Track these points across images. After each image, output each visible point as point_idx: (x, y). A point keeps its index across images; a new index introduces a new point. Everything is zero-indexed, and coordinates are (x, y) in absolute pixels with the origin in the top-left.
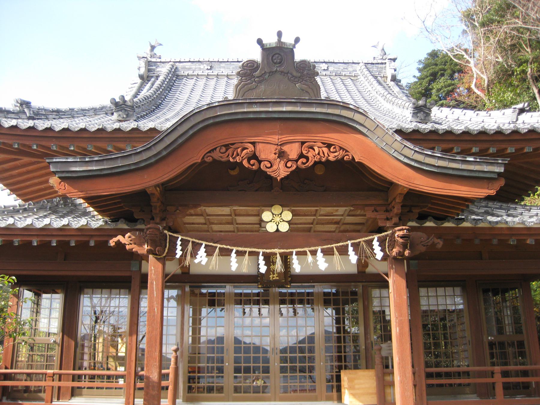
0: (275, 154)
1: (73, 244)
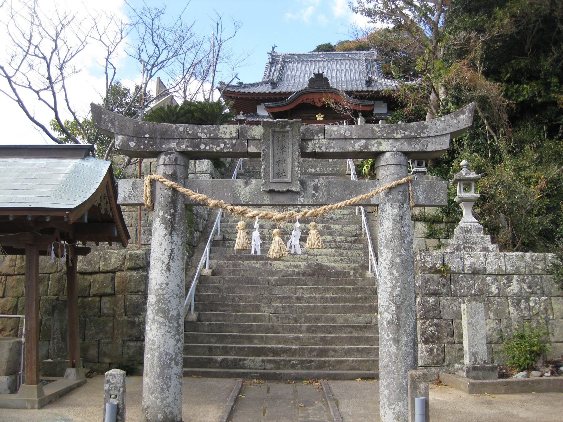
0: (317, 100)
1: (48, 219)
